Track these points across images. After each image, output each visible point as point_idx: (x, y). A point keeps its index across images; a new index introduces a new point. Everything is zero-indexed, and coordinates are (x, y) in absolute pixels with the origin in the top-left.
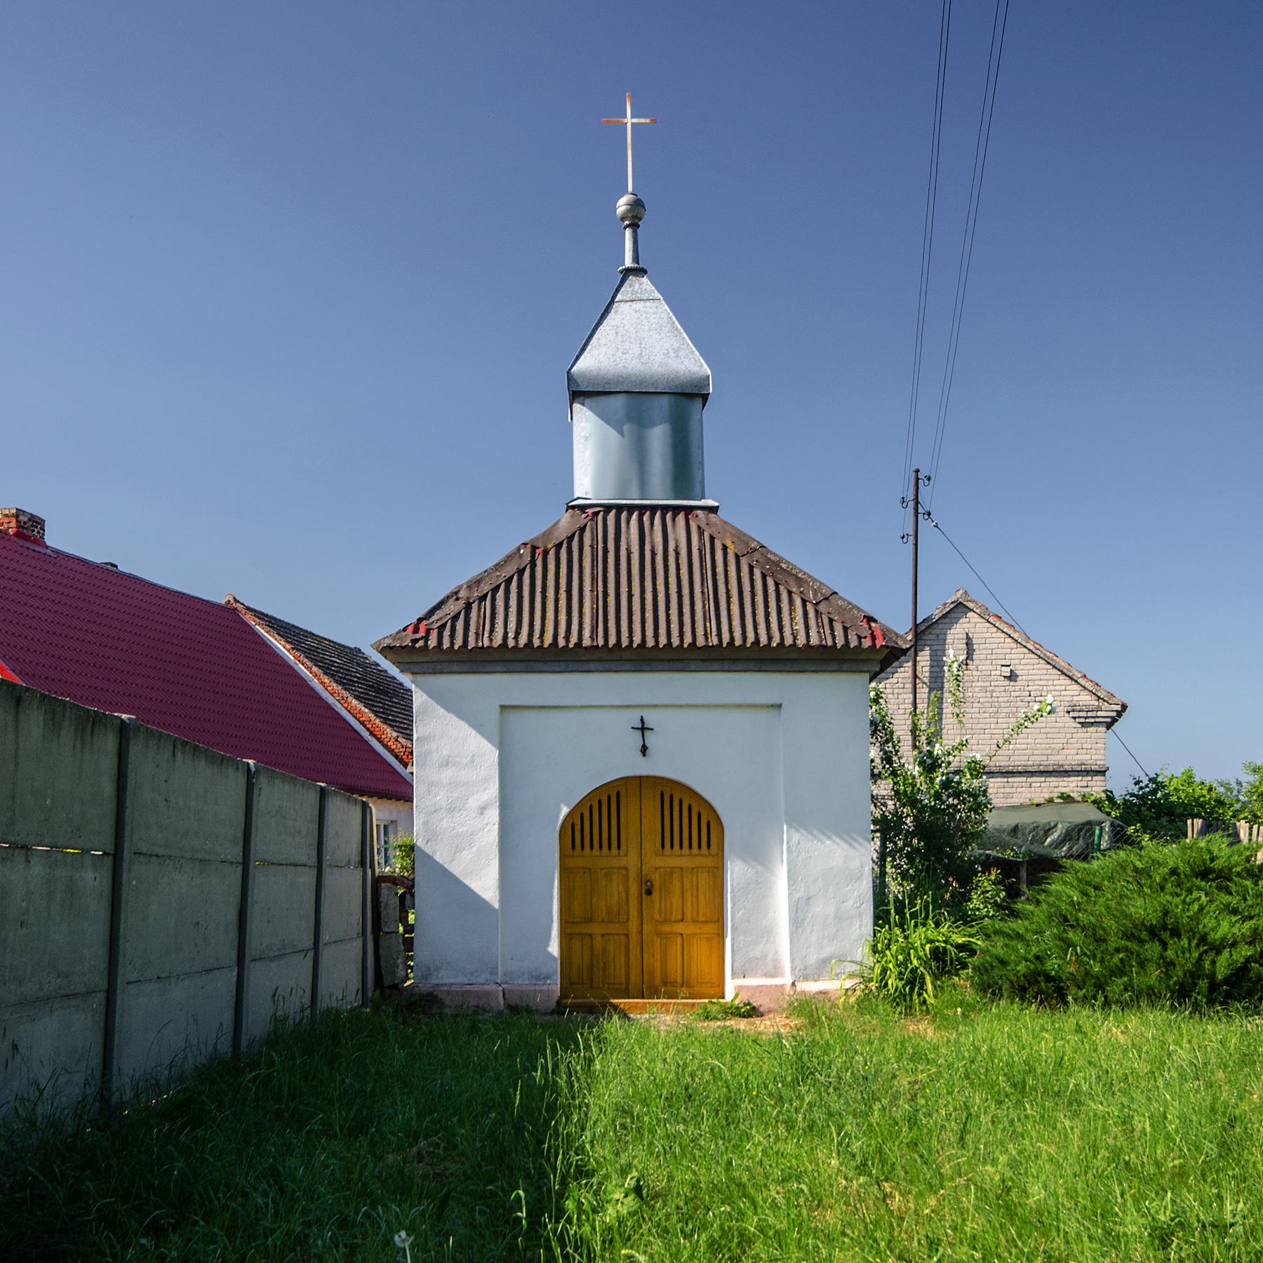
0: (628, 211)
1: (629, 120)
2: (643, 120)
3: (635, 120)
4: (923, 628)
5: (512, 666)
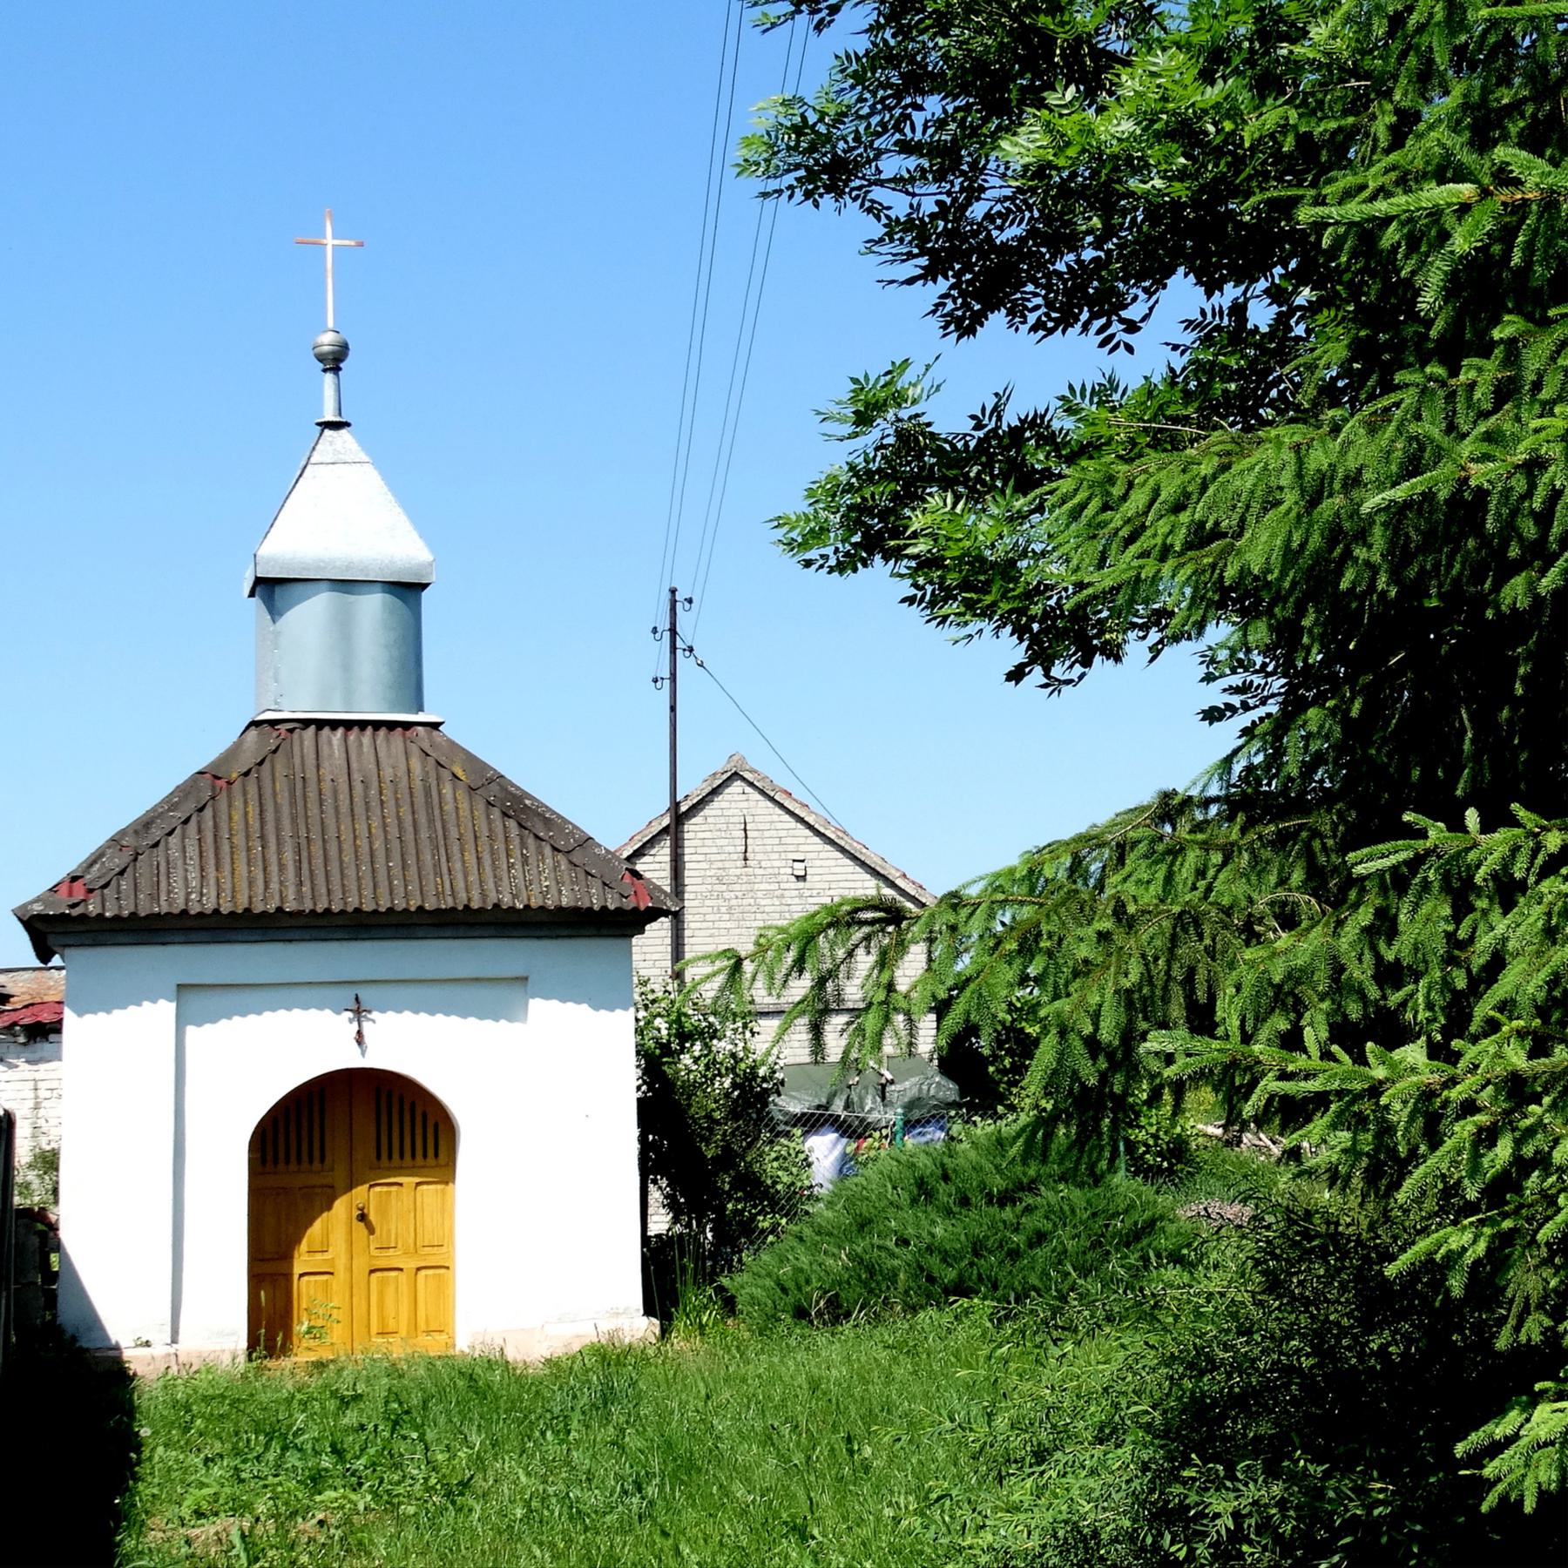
0: (333, 353)
1: (330, 241)
2: (347, 242)
3: (337, 242)
4: (684, 808)
5: (193, 936)
